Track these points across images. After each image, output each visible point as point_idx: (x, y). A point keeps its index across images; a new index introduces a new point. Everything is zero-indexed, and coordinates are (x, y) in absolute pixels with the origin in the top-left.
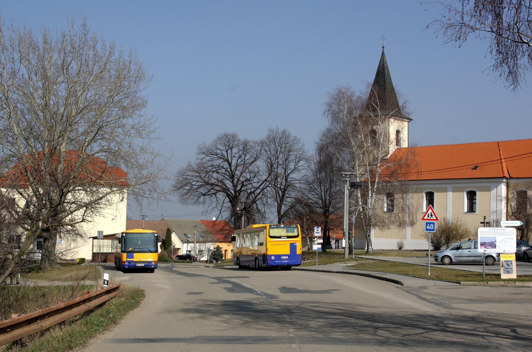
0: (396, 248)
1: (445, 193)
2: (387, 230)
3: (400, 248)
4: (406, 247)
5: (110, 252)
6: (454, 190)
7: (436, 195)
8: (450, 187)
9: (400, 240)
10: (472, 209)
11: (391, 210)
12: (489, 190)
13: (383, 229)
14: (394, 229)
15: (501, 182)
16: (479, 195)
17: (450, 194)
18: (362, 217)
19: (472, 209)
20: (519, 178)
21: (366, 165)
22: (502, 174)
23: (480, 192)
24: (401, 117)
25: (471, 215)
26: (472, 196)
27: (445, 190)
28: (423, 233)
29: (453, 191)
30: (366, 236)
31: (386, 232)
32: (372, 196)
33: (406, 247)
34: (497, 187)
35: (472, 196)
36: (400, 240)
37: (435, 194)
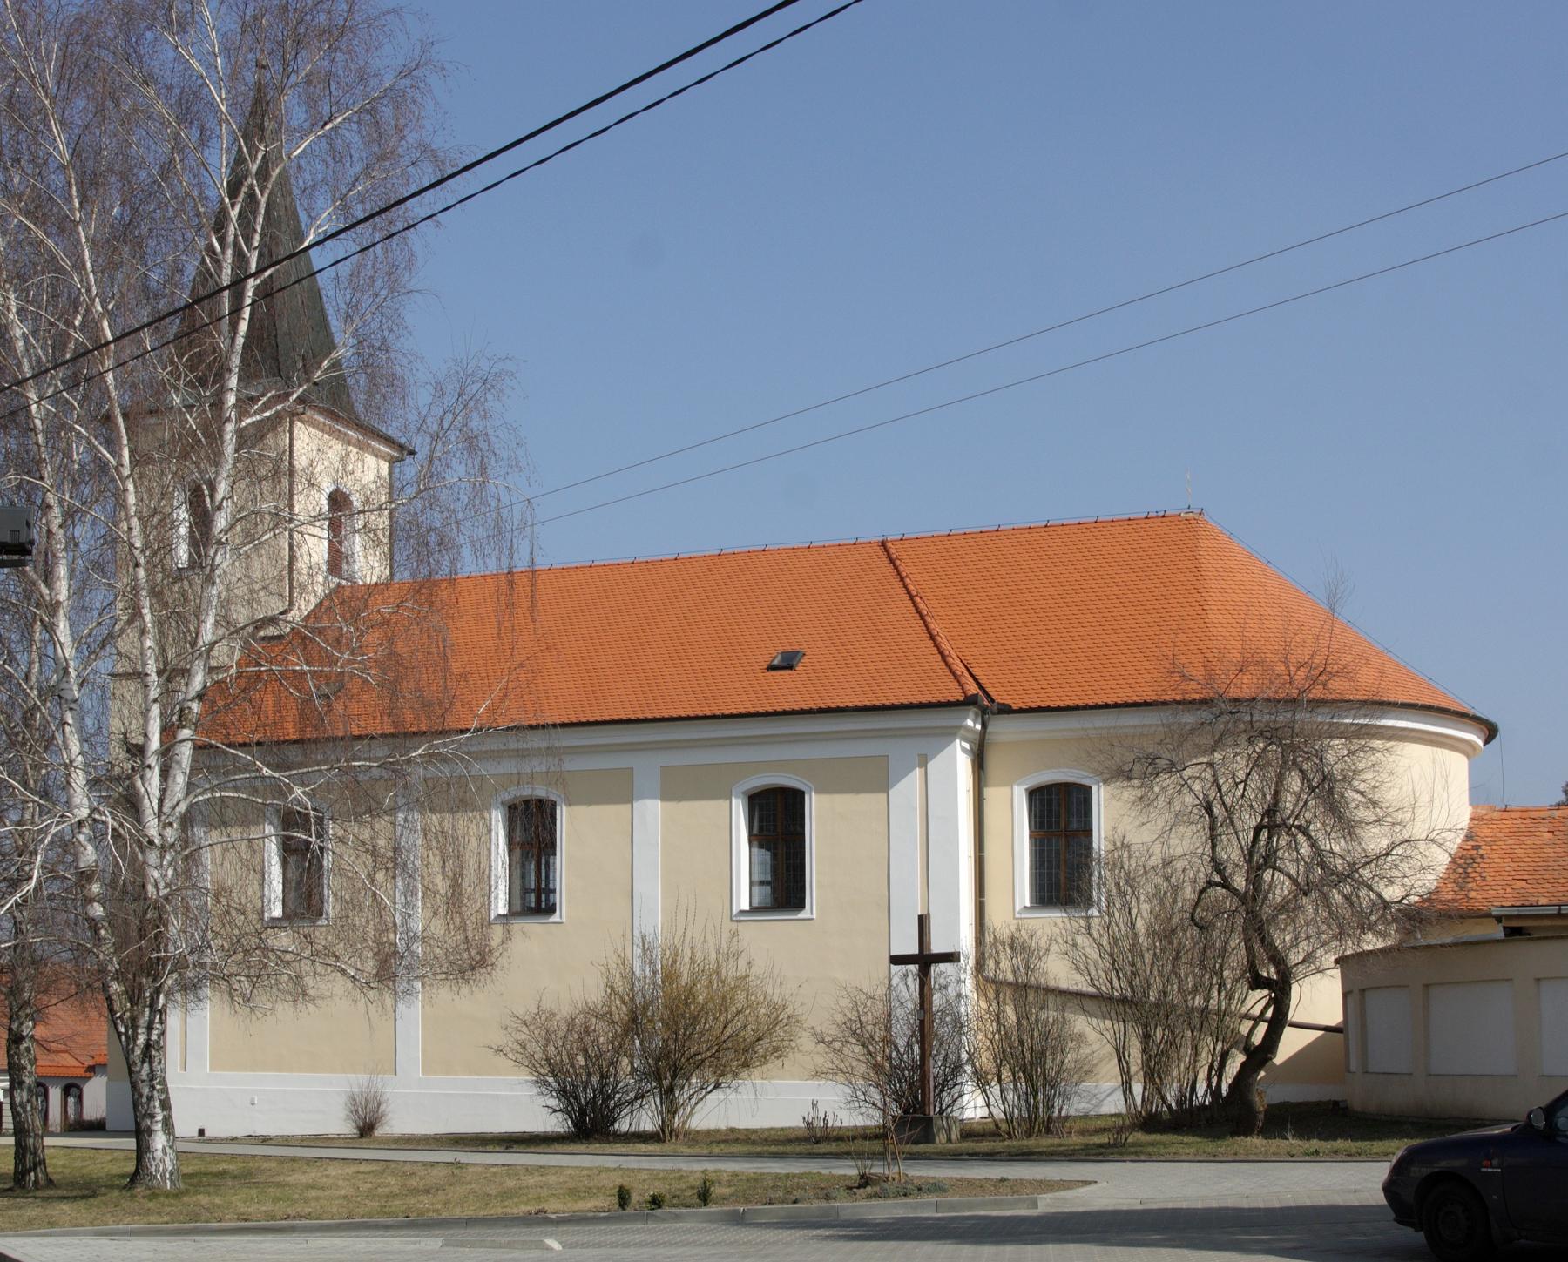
0: (340, 1125)
1: (624, 809)
2: (284, 1009)
3: (366, 1129)
4: (397, 1123)
5: (11, 1141)
6: (675, 788)
7: (568, 822)
8: (647, 767)
9: (363, 1078)
10: (785, 888)
11: (305, 899)
12: (878, 779)
13: (261, 999)
14: (338, 1002)
15: (950, 733)
16: (823, 817)
17: (651, 812)
18: (97, 910)
19: (785, 888)
20: (1048, 709)
21: (140, 676)
22: (953, 685)
23: (825, 798)
24: (334, 416)
25: (780, 927)
26: (778, 822)
27: (621, 791)
28: (499, 1038)
29: (666, 796)
30: (128, 1052)
31: (282, 1020)
32: (167, 752)
33: (397, 1123)
34: (923, 762)
35: (778, 822)
36: (363, 1078)
37: (564, 815)
